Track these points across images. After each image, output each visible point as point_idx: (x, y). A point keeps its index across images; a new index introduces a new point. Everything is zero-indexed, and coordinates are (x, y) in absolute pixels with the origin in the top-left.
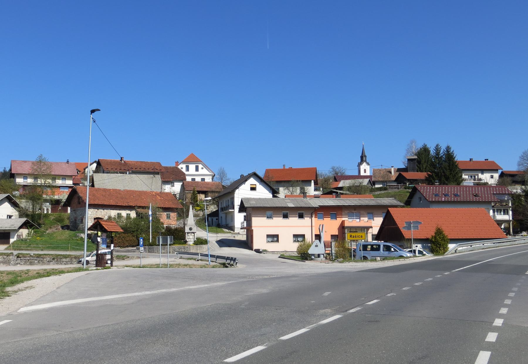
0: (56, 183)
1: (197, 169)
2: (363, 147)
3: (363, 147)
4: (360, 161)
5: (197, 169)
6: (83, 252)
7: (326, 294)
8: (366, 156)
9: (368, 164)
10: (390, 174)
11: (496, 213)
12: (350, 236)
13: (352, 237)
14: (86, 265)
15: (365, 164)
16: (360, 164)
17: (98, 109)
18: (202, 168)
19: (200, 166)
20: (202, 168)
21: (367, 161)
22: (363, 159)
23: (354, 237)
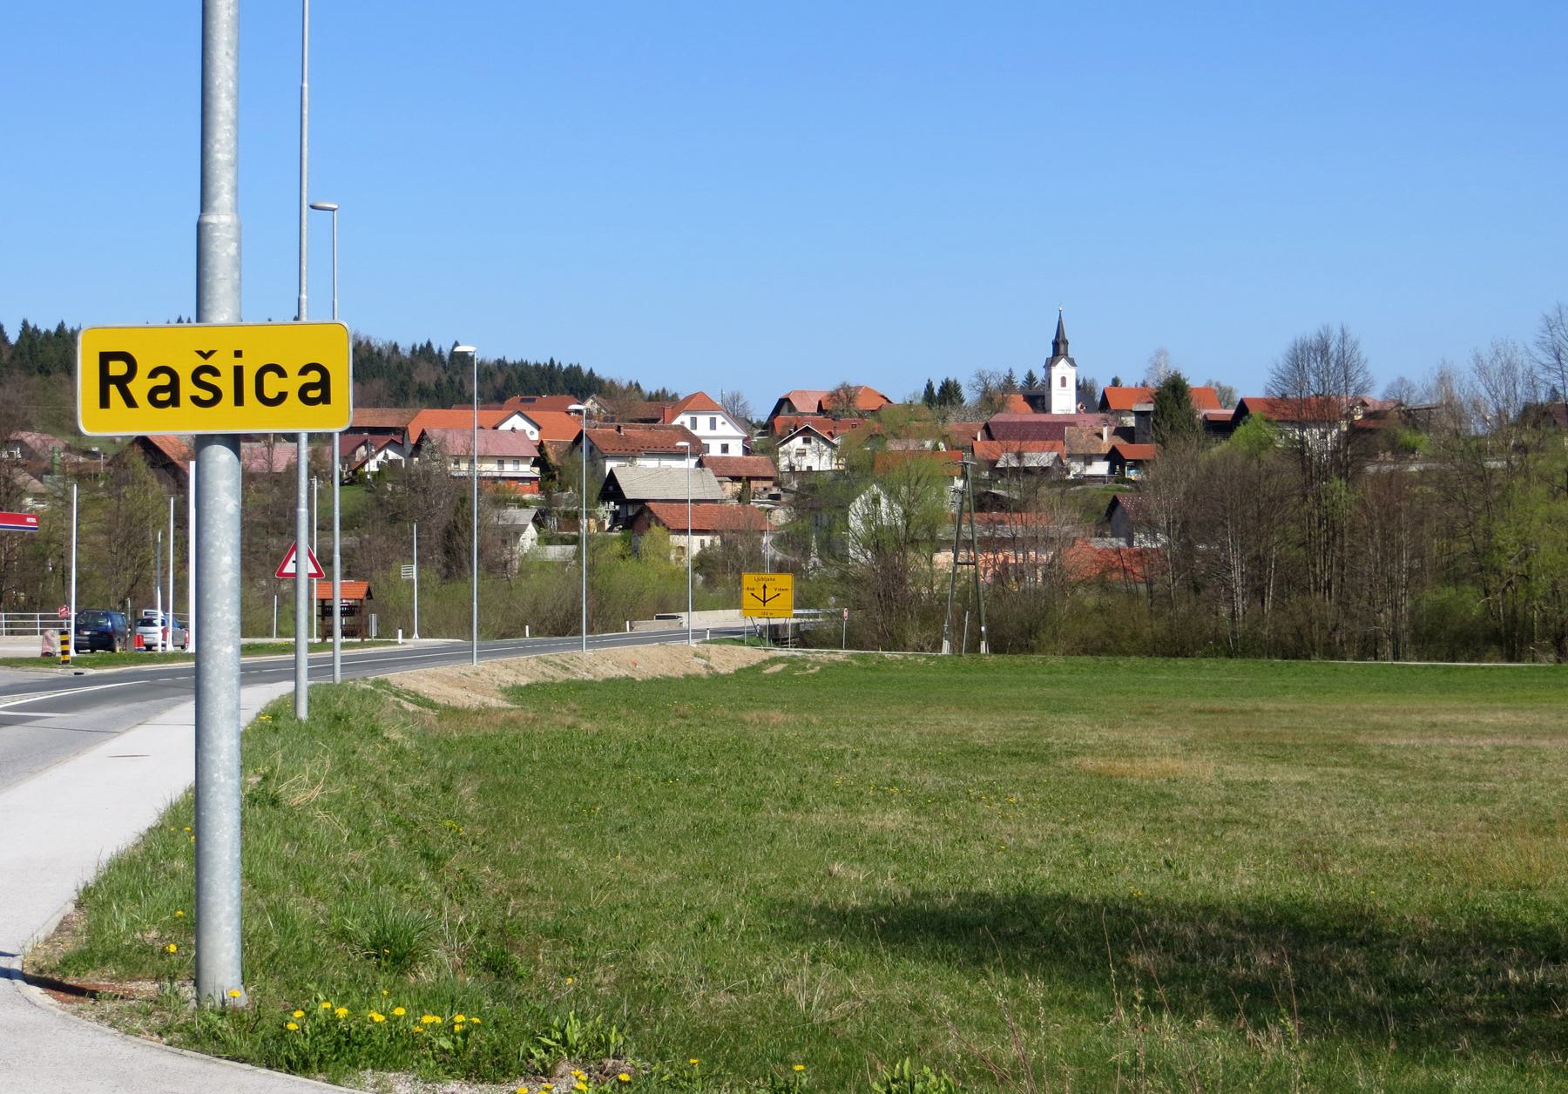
0: (975, 511)
1: (713, 425)
2: (1060, 323)
3: (1060, 323)
4: (1050, 354)
5: (713, 425)
6: (294, 639)
7: (983, 629)
8: (1066, 343)
9: (1072, 363)
10: (1100, 440)
11: (1483, 391)
12: (106, 380)
13: (140, 387)
14: (249, 676)
15: (1063, 363)
16: (1052, 362)
17: (565, 361)
18: (723, 423)
19: (719, 419)
20: (723, 423)
21: (1070, 356)
22: (1059, 348)
23: (167, 395)
